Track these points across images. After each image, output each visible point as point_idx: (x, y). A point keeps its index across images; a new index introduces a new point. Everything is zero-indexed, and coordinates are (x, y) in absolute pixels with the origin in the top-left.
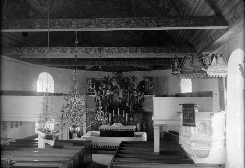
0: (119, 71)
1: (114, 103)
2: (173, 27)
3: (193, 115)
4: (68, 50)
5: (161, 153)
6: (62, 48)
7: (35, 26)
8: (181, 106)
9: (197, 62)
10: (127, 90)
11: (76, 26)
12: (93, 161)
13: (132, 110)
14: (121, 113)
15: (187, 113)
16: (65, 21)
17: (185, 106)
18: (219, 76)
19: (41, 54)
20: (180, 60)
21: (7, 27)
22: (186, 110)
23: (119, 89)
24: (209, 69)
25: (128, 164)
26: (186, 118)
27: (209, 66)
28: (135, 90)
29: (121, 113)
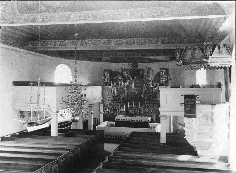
0: (135, 62)
1: (130, 94)
2: (168, 17)
3: (193, 106)
4: (78, 42)
5: (168, 143)
6: (73, 40)
7: (37, 19)
8: (183, 97)
9: (198, 53)
10: (142, 81)
11: (74, 19)
12: (105, 149)
13: (147, 101)
14: (137, 104)
15: (189, 104)
16: (64, 14)
17: (186, 97)
18: (225, 66)
19: (54, 46)
20: (181, 51)
21: (13, 21)
22: (187, 101)
23: (132, 80)
24: (210, 59)
25: (131, 153)
26: (187, 109)
27: (210, 56)
28: (150, 81)
29: (137, 104)
